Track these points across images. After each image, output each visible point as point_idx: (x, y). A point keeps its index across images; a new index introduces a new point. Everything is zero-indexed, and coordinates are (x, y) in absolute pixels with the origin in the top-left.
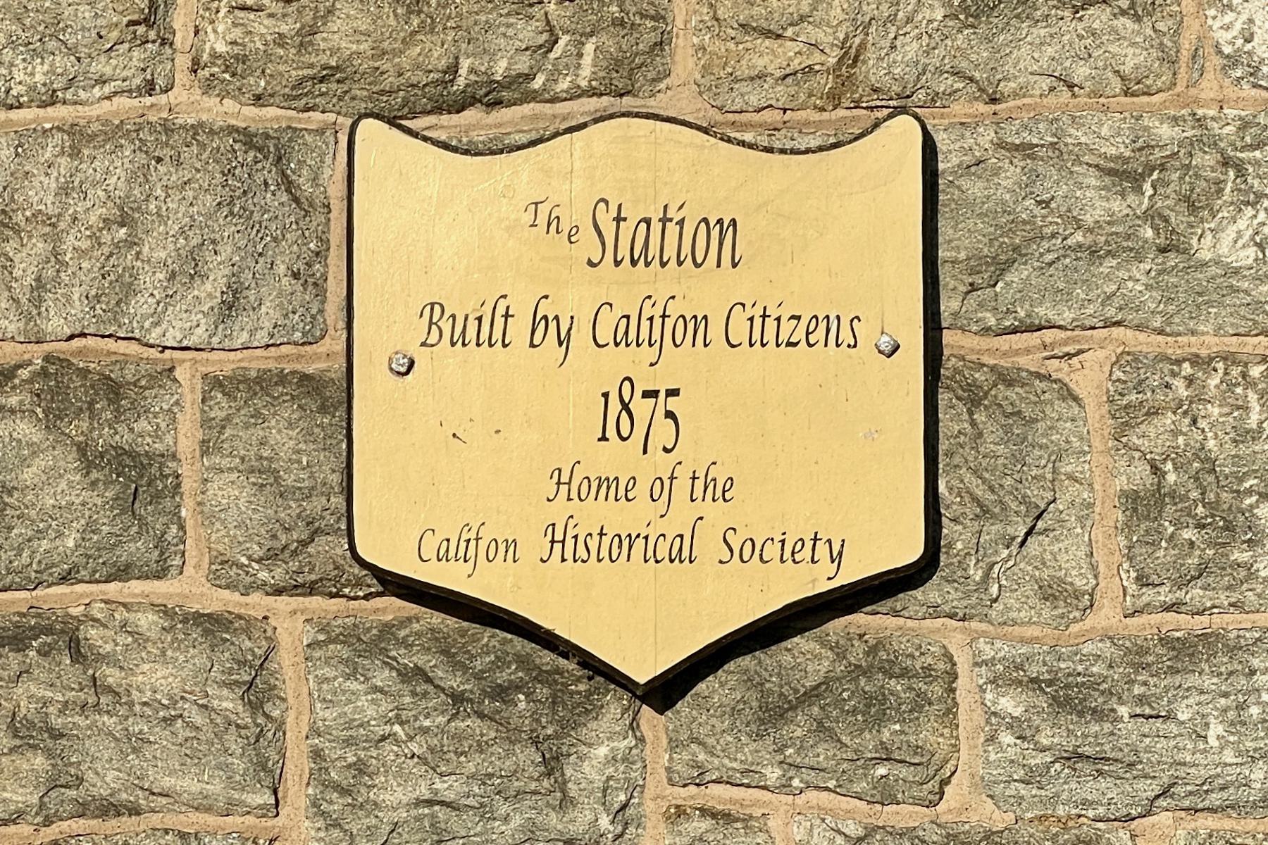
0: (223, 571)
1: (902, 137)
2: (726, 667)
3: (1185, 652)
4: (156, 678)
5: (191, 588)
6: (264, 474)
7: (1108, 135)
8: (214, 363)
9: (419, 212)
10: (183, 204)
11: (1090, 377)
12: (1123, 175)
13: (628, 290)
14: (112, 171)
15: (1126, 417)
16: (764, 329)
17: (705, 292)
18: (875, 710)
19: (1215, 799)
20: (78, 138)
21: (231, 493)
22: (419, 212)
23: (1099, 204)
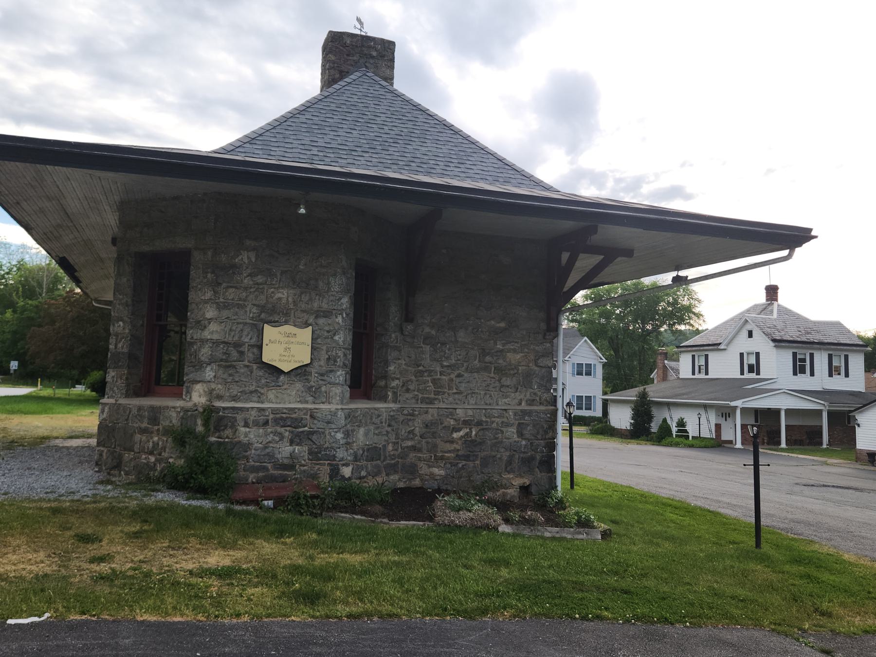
0: (249, 361)
1: (310, 327)
2: (17, 163)
3: (331, 371)
4: (242, 371)
5: (246, 363)
6: (253, 353)
7: (327, 328)
8: (188, 591)
9: (269, 332)
10: (247, 329)
11: (324, 348)
12: (328, 332)
13: (287, 339)
14: (241, 326)
15: (327, 352)
16: (298, 343)
17: (292, 340)
18: (305, 375)
19: (784, 628)
20: (238, 323)
21: (251, 355)
22: (269, 332)
23: (326, 334)
